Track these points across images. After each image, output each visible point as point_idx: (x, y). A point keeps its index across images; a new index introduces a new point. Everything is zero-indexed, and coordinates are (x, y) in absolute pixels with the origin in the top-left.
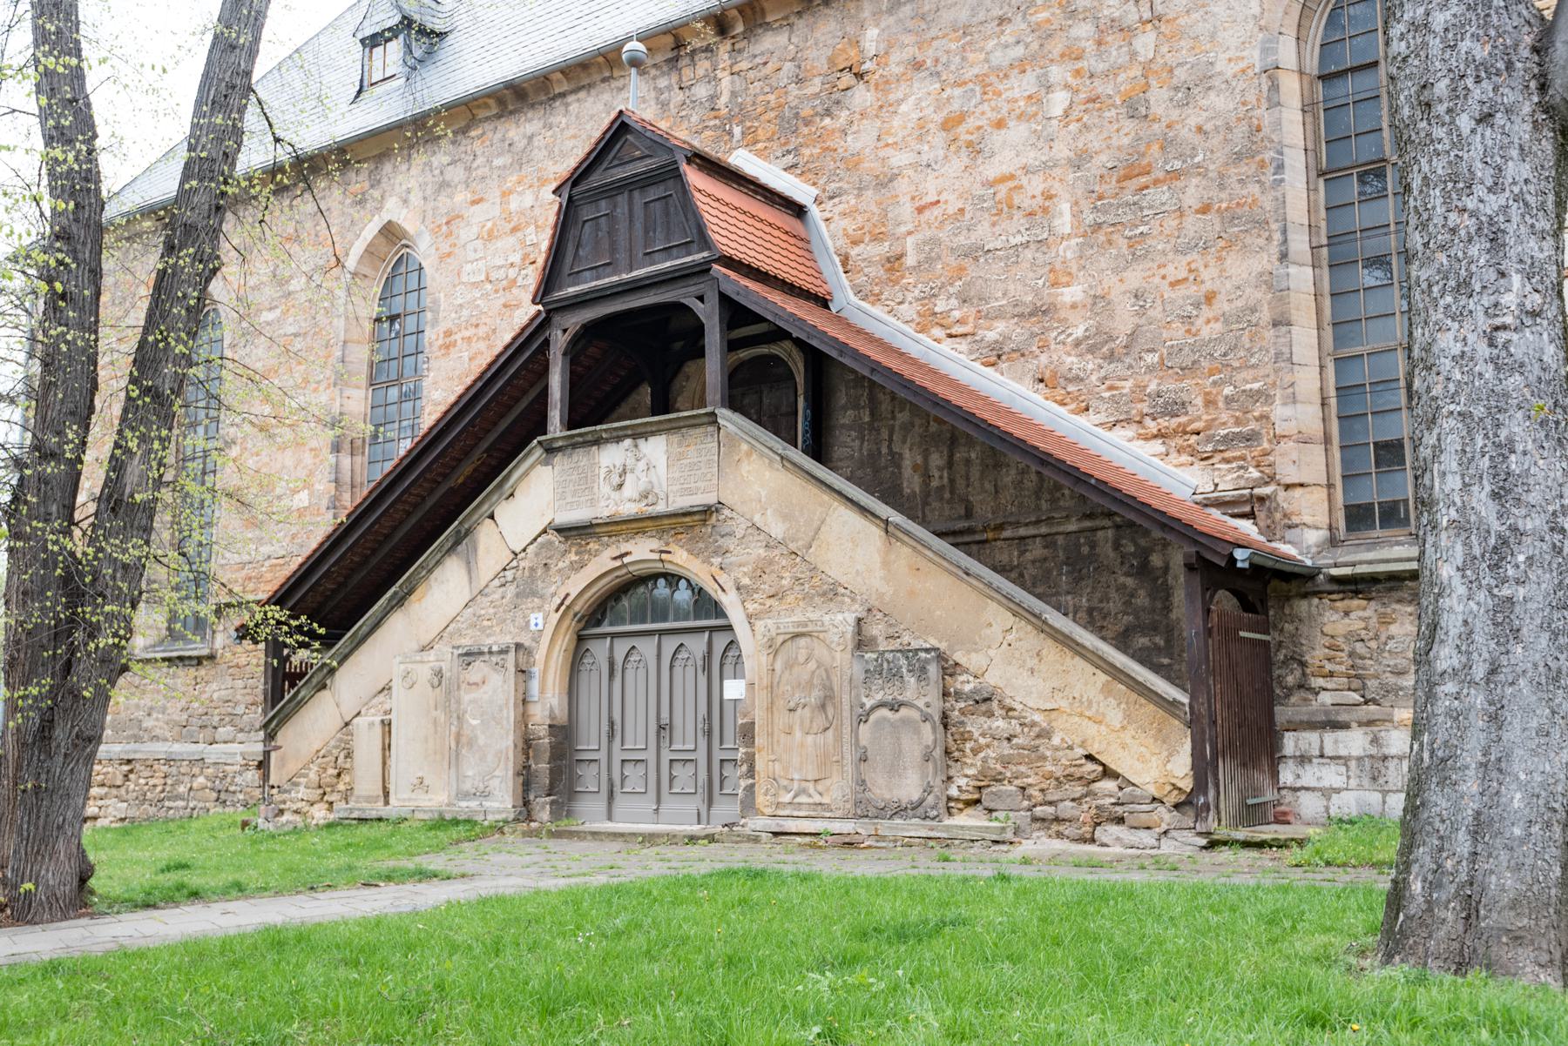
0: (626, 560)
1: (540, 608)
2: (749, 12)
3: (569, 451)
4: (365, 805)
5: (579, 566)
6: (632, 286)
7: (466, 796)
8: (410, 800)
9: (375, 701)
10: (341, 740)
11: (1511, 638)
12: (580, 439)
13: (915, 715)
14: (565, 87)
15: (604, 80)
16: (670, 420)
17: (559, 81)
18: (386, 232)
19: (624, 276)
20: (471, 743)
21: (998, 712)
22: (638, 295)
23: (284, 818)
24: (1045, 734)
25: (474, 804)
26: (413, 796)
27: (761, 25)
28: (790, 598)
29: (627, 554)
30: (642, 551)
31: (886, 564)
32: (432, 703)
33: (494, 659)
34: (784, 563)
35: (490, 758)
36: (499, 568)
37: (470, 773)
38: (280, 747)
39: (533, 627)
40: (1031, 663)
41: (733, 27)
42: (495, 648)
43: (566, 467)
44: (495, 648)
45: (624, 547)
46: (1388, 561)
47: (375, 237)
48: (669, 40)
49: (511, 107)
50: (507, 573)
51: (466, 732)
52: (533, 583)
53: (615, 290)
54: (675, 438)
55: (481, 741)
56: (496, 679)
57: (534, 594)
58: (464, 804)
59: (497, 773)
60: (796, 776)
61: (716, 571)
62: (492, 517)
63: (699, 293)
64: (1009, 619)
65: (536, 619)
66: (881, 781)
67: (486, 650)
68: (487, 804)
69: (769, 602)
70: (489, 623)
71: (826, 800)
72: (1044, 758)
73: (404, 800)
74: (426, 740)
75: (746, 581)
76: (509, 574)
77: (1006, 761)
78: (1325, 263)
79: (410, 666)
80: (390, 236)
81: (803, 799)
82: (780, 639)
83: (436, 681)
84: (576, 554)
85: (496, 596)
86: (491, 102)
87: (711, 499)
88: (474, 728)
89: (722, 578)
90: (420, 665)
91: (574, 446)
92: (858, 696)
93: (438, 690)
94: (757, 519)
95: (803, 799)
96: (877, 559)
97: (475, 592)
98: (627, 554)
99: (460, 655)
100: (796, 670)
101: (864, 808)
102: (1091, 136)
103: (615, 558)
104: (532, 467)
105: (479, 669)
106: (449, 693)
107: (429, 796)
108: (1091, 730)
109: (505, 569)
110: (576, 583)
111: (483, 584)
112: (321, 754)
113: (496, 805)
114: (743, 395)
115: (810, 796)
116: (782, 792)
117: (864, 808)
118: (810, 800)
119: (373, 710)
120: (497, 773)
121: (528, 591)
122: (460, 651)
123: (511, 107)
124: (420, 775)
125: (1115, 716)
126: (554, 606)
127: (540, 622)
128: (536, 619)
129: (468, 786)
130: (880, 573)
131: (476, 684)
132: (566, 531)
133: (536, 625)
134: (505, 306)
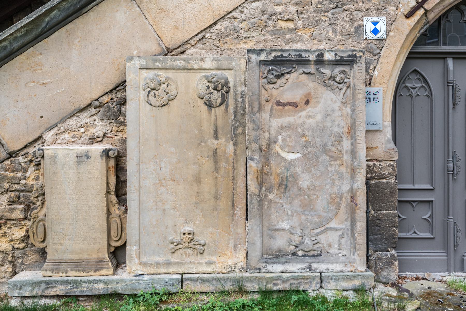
4: (73, 275)
8: (168, 264)
9: (72, 122)
11: (76, 128)
26: (175, 259)
32: (208, 129)
33: (327, 71)
37: (284, 225)
42: (328, 56)
44: (328, 56)
59: (333, 224)
67: (313, 58)
70: (291, 25)
73: (158, 264)
79: (163, 75)
83: (216, 97)
88: (290, 164)
90: (181, 75)
93: (220, 111)
107: (206, 258)
113: (338, 267)
120: (333, 224)
122: (263, 57)
124: (188, 229)
127: (382, 27)
131: (295, 105)
133: (375, 32)
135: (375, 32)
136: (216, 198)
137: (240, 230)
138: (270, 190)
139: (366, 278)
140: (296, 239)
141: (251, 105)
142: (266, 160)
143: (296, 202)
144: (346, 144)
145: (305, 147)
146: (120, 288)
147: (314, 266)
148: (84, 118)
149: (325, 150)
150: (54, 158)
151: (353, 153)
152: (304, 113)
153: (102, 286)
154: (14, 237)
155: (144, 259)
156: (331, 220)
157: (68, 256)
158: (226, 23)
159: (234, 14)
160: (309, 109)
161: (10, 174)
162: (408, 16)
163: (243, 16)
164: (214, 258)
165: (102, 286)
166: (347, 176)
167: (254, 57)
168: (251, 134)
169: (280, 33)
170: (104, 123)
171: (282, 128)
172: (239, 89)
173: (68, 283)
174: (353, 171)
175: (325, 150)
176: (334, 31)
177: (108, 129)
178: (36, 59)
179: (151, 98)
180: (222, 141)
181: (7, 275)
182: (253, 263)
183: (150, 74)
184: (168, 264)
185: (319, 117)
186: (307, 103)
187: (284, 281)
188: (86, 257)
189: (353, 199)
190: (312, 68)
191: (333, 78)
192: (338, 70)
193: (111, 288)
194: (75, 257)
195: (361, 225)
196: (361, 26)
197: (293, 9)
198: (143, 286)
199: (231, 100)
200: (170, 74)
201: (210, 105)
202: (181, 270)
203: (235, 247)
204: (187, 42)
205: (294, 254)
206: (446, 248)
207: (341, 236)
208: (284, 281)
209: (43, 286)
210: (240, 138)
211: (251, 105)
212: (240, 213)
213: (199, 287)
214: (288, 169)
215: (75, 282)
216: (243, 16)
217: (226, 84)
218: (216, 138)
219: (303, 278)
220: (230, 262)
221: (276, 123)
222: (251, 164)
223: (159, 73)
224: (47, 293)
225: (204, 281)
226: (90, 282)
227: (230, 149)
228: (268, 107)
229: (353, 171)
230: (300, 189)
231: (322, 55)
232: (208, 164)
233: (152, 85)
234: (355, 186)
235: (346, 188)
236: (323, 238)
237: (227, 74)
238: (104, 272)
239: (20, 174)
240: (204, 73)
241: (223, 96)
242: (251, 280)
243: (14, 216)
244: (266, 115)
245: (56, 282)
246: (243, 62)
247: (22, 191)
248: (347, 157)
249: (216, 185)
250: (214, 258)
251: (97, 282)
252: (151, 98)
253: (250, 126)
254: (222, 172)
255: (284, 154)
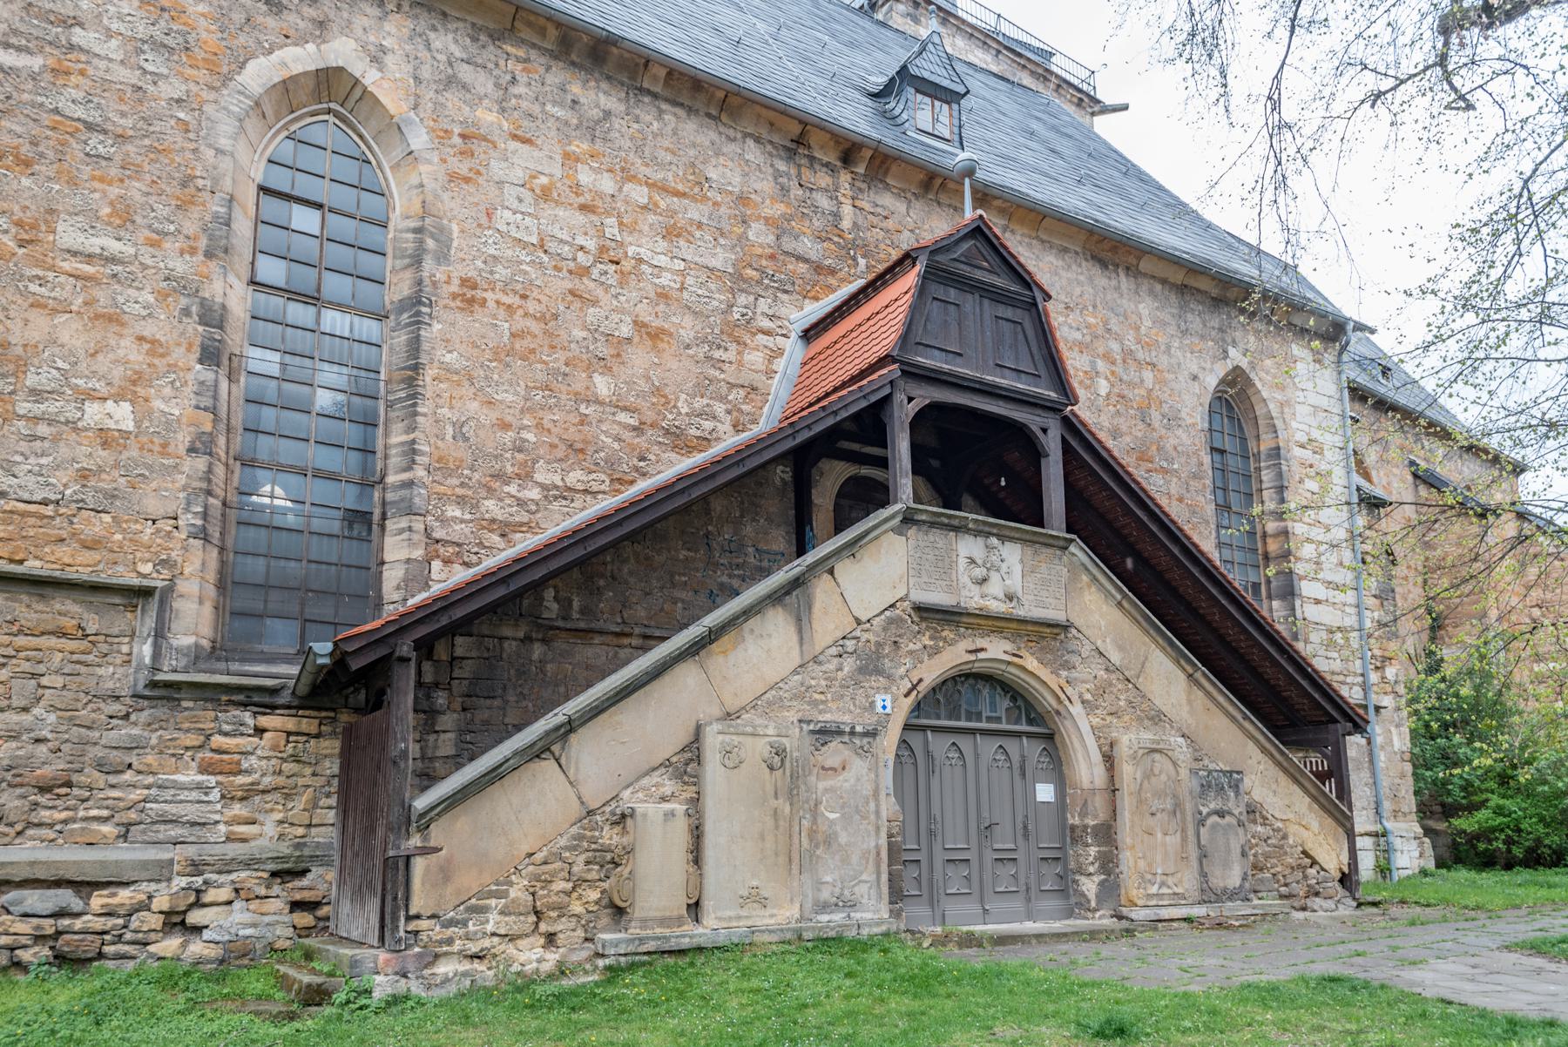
0: (981, 655)
1: (886, 690)
2: (877, 162)
3: (925, 528)
5: (935, 652)
6: (990, 389)
7: (824, 907)
8: (739, 918)
9: (645, 781)
10: (580, 838)
12: (946, 521)
13: (1235, 822)
14: (658, 89)
15: (709, 115)
16: (1036, 533)
17: (655, 78)
18: (322, 76)
19: (997, 380)
20: (829, 841)
21: (1260, 820)
22: (987, 400)
23: (444, 968)
24: (1285, 837)
25: (838, 917)
26: (744, 913)
27: (881, 181)
28: (1126, 718)
29: (982, 650)
30: (996, 649)
31: (1189, 702)
32: (770, 789)
33: (857, 741)
34: (1120, 686)
35: (855, 859)
36: (840, 634)
37: (828, 878)
38: (437, 850)
39: (879, 709)
40: (1274, 786)
41: (856, 165)
42: (859, 729)
43: (922, 544)
44: (859, 729)
45: (980, 643)
46: (256, 675)
47: (305, 74)
48: (796, 129)
49: (574, 57)
50: (847, 642)
51: (823, 827)
52: (878, 659)
53: (972, 385)
54: (1029, 551)
55: (843, 838)
56: (859, 766)
57: (879, 672)
58: (824, 918)
60: (1159, 871)
61: (1063, 683)
62: (831, 572)
63: (1045, 426)
64: (1261, 756)
65: (883, 701)
66: (1218, 873)
67: (847, 729)
68: (856, 915)
69: (1109, 718)
70: (822, 697)
71: (1179, 890)
72: (1286, 853)
73: (730, 918)
74: (762, 837)
75: (1088, 696)
76: (850, 645)
77: (1267, 856)
78: (379, 455)
80: (323, 86)
81: (1165, 890)
82: (1141, 752)
84: (931, 638)
85: (831, 666)
86: (553, 32)
87: (1058, 615)
88: (832, 822)
89: (1069, 691)
90: (749, 739)
91: (932, 525)
92: (1196, 805)
94: (1099, 643)
95: (1165, 890)
96: (1183, 696)
97: (807, 658)
98: (982, 650)
99: (813, 732)
100: (1153, 780)
101: (1210, 895)
102: (1122, 420)
103: (970, 652)
104: (886, 532)
105: (835, 752)
106: (794, 777)
107: (769, 912)
108: (1305, 834)
109: (844, 638)
110: (932, 672)
111: (818, 649)
112: (539, 857)
113: (868, 916)
114: (851, 507)
115: (1169, 887)
116: (1149, 885)
117: (1210, 895)
118: (1170, 891)
119: (640, 795)
120: (864, 877)
121: (871, 666)
122: (812, 727)
123: (574, 57)
124: (755, 883)
125: (1315, 825)
126: (904, 690)
127: (888, 704)
128: (883, 701)
129: (825, 895)
130: (1186, 708)
131: (834, 770)
132: (923, 611)
133: (884, 707)
134: (572, 292)
135: (884, 707)
136: (776, 854)
137: (795, 884)
138: (817, 846)
139: (890, 923)
140: (837, 891)
141: (803, 770)
142: (814, 821)
143: (837, 857)
144: (872, 805)
145: (842, 807)
146: (702, 942)
147: (852, 915)
148: (655, 778)
149: (858, 811)
150: (645, 815)
151: (877, 813)
152: (841, 778)
153: (687, 940)
154: (590, 899)
155: (719, 914)
156: (862, 873)
157: (652, 914)
158: (774, 692)
159: (780, 685)
160: (845, 774)
161: (589, 834)
162: (906, 695)
163: (787, 687)
164: (775, 911)
165: (687, 940)
166: (873, 833)
167: (805, 726)
168: (803, 795)
169: (814, 703)
170: (672, 782)
171: (826, 790)
172: (795, 754)
173: (659, 938)
174: (878, 829)
175: (858, 811)
176: (855, 705)
177: (674, 789)
178: (616, 718)
179: (726, 761)
180: (781, 801)
181: (580, 941)
182: (807, 915)
183: (727, 738)
184: (739, 918)
185: (852, 781)
186: (844, 768)
187: (832, 929)
188: (668, 914)
189: (878, 854)
190: (846, 739)
191: (862, 747)
192: (866, 740)
193: (696, 942)
194: (658, 914)
195: (885, 877)
196: (873, 702)
197: (824, 683)
198: (721, 939)
199: (788, 764)
200: (741, 738)
201: (771, 768)
202: (750, 924)
203: (792, 900)
204: (743, 708)
205: (836, 905)
206: (932, 904)
207: (870, 888)
208: (832, 929)
209: (637, 942)
210: (796, 798)
211: (803, 770)
212: (795, 868)
213: (766, 938)
214: (830, 827)
215: (665, 937)
216: (787, 687)
217: (784, 750)
218: (776, 798)
219: (846, 926)
220: (788, 914)
221: (821, 785)
222: (804, 822)
223: (734, 737)
224: (640, 950)
225: (771, 932)
226: (677, 937)
227: (787, 809)
228: (815, 771)
229: (878, 829)
230: (839, 845)
231: (853, 727)
232: (770, 822)
233: (728, 749)
234: (880, 842)
235: (873, 844)
236: (856, 889)
237: (784, 740)
238: (685, 927)
239: (597, 834)
240: (768, 739)
241: (782, 760)
242: (807, 929)
243: (589, 877)
244: (813, 779)
245: (648, 938)
246: (797, 730)
247: (599, 851)
248: (873, 817)
249: (776, 842)
250: (775, 911)
251: (684, 936)
252: (726, 761)
253: (803, 787)
254: (781, 829)
255: (827, 814)
